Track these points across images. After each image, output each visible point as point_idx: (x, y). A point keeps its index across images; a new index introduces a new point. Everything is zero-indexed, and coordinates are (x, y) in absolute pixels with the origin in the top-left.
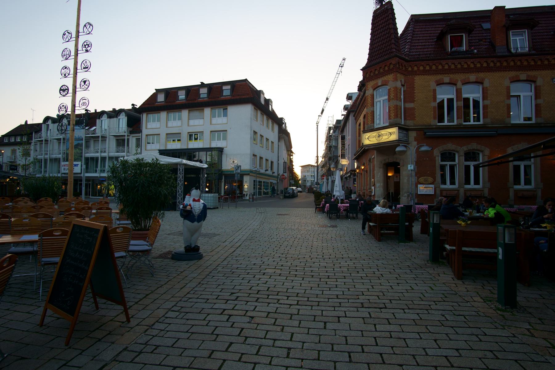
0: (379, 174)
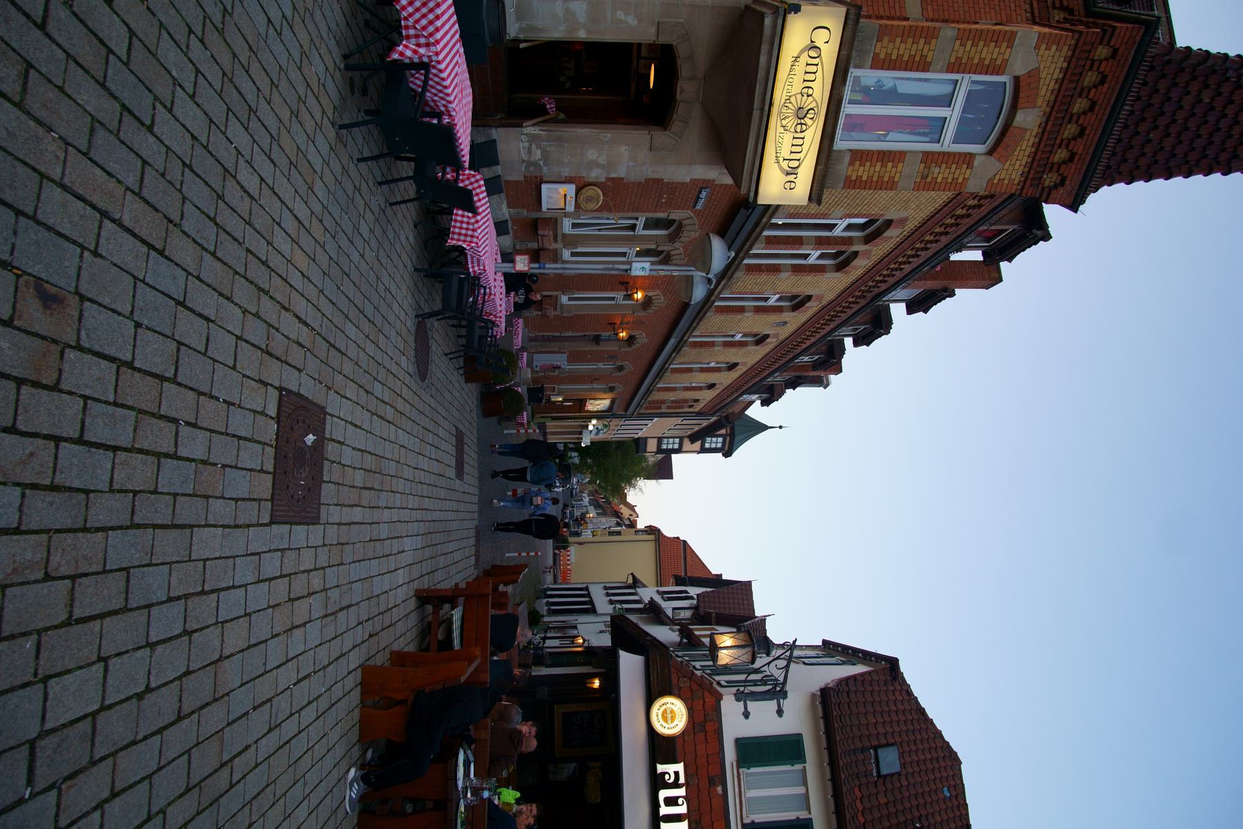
0: (632, 21)
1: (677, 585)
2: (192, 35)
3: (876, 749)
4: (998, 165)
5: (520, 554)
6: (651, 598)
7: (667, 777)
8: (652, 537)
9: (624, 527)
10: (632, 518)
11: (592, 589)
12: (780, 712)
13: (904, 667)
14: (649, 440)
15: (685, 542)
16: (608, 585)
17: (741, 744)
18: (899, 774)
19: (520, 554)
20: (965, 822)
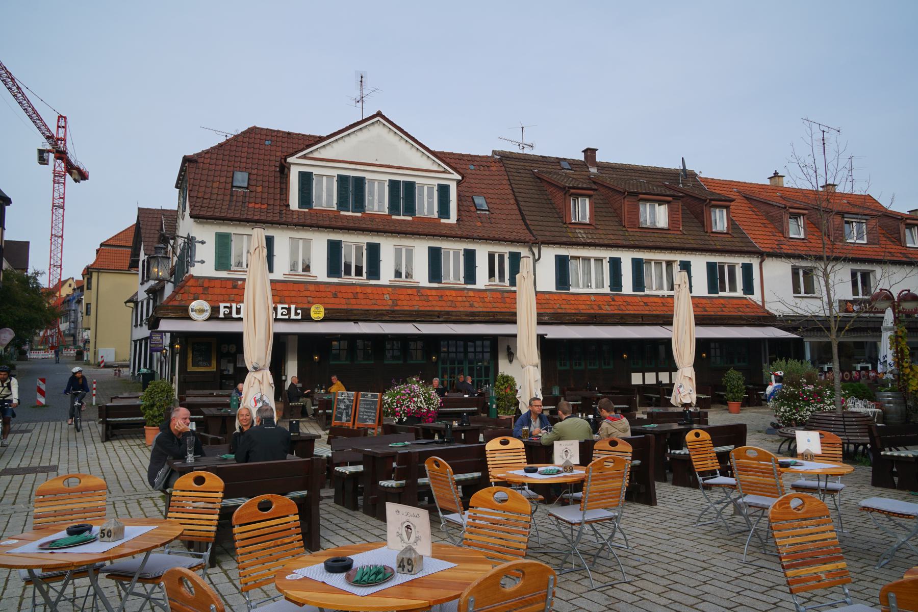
1: (138, 267)
3: (233, 186)
5: (94, 395)
6: (145, 291)
7: (226, 312)
8: (95, 275)
9: (83, 297)
10: (74, 286)
11: (136, 337)
12: (203, 243)
13: (190, 153)
15: (102, 245)
16: (134, 324)
17: (218, 268)
18: (250, 174)
19: (94, 395)
20: (286, 135)
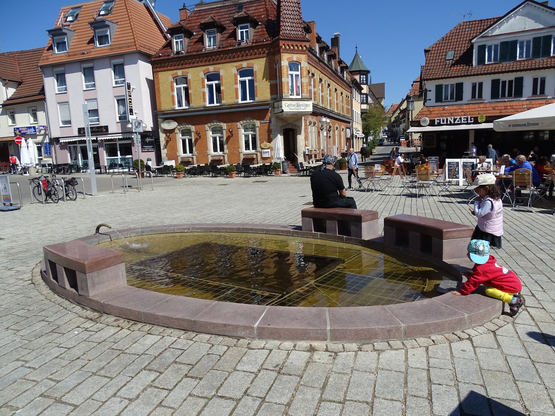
2: (73, 408)
4: (303, 61)
12: (430, 91)
14: (362, 108)
